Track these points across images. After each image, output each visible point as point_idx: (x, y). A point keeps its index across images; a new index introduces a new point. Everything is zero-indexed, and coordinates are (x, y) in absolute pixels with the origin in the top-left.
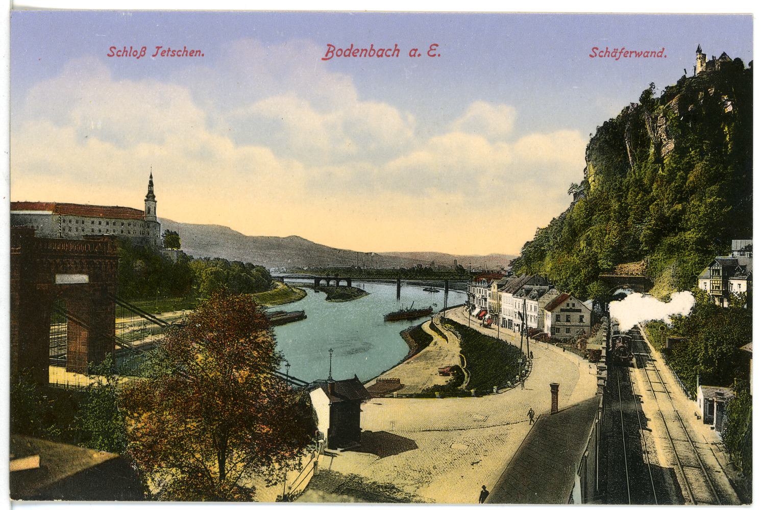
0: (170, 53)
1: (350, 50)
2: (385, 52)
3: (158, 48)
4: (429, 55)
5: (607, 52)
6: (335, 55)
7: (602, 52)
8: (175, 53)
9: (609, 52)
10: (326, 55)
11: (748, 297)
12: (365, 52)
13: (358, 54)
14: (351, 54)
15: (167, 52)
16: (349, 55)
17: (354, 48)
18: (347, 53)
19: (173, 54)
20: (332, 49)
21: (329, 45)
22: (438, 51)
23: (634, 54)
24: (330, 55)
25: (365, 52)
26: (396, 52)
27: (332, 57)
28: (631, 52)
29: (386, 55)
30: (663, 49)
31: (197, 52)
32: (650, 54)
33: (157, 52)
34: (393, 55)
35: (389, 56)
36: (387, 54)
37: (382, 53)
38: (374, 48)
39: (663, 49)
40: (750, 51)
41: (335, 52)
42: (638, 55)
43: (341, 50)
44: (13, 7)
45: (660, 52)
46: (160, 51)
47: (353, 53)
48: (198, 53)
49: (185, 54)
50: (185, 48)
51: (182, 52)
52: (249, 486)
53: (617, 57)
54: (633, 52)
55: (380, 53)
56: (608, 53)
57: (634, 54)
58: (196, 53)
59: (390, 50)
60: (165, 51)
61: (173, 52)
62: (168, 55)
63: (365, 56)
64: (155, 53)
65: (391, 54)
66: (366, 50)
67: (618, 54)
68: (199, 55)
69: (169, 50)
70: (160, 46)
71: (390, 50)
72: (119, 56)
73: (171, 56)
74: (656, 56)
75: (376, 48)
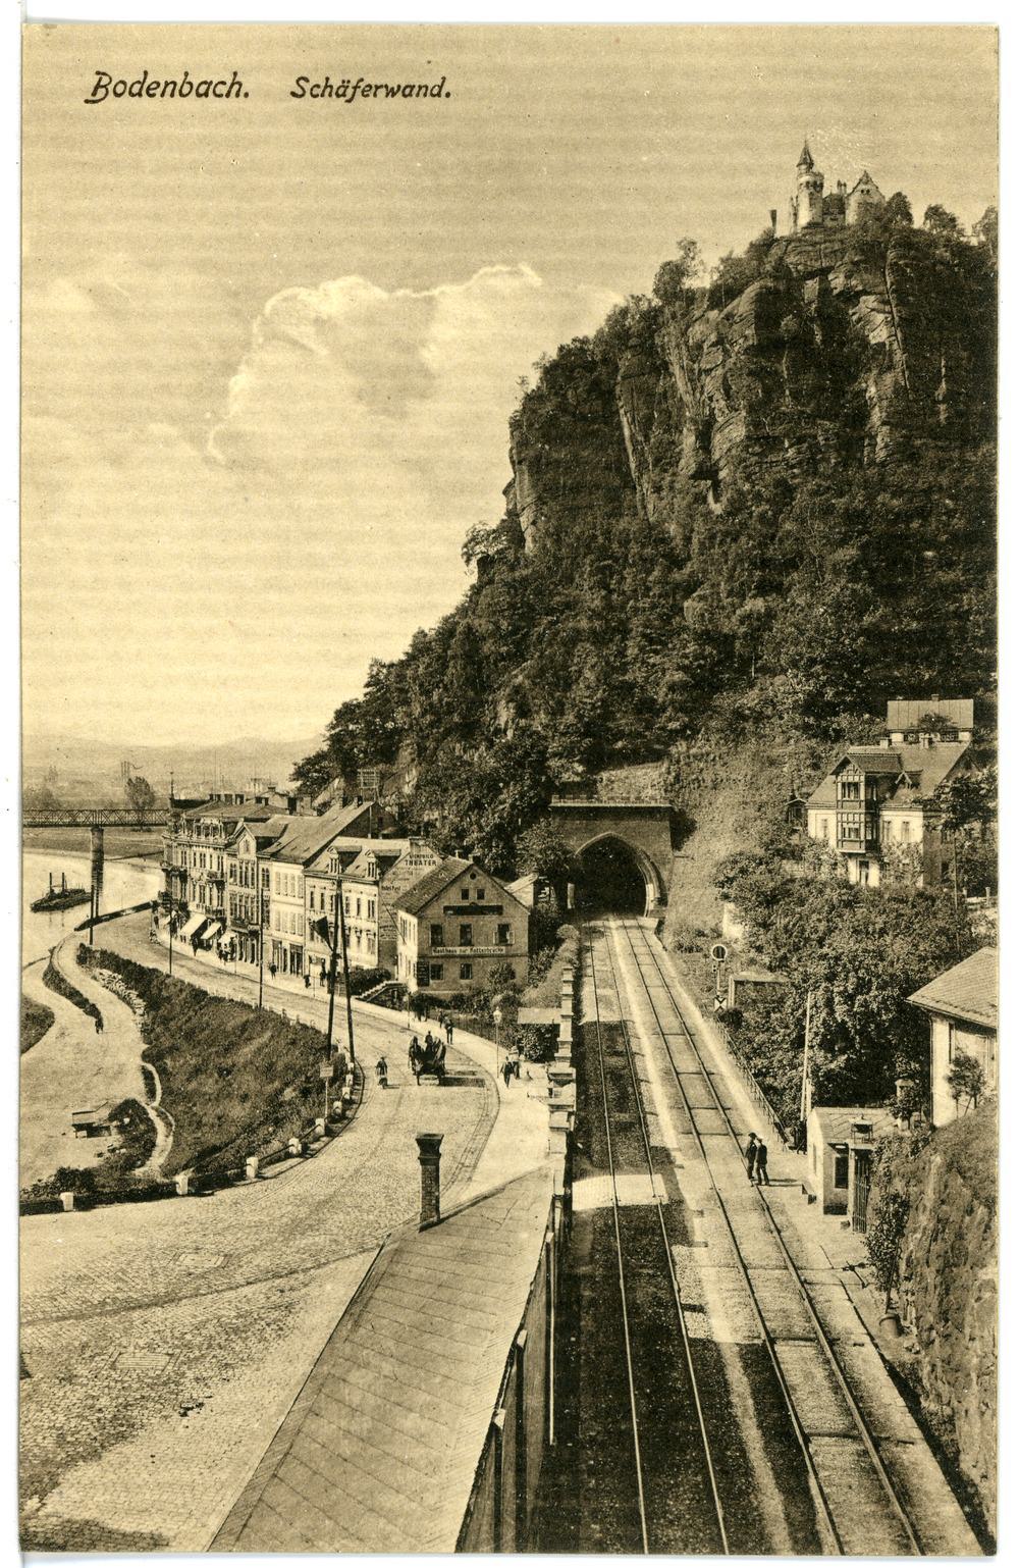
1: (441, 87)
2: (212, 87)
5: (326, 86)
8: (307, 87)
9: (331, 87)
10: (94, 94)
13: (159, 91)
16: (140, 94)
18: (135, 90)
19: (300, 92)
20: (105, 80)
21: (98, 73)
23: (382, 92)
24: (101, 92)
25: (171, 86)
26: (236, 87)
28: (377, 87)
29: (147, 93)
30: (444, 79)
32: (416, 90)
34: (228, 95)
35: (220, 96)
36: (218, 92)
37: (205, 90)
39: (444, 79)
41: (110, 87)
42: (391, 92)
47: (148, 88)
53: (349, 96)
54: (381, 86)
55: (203, 89)
56: (328, 90)
57: (382, 92)
59: (223, 83)
65: (225, 93)
67: (350, 92)
68: (237, 95)
71: (223, 83)
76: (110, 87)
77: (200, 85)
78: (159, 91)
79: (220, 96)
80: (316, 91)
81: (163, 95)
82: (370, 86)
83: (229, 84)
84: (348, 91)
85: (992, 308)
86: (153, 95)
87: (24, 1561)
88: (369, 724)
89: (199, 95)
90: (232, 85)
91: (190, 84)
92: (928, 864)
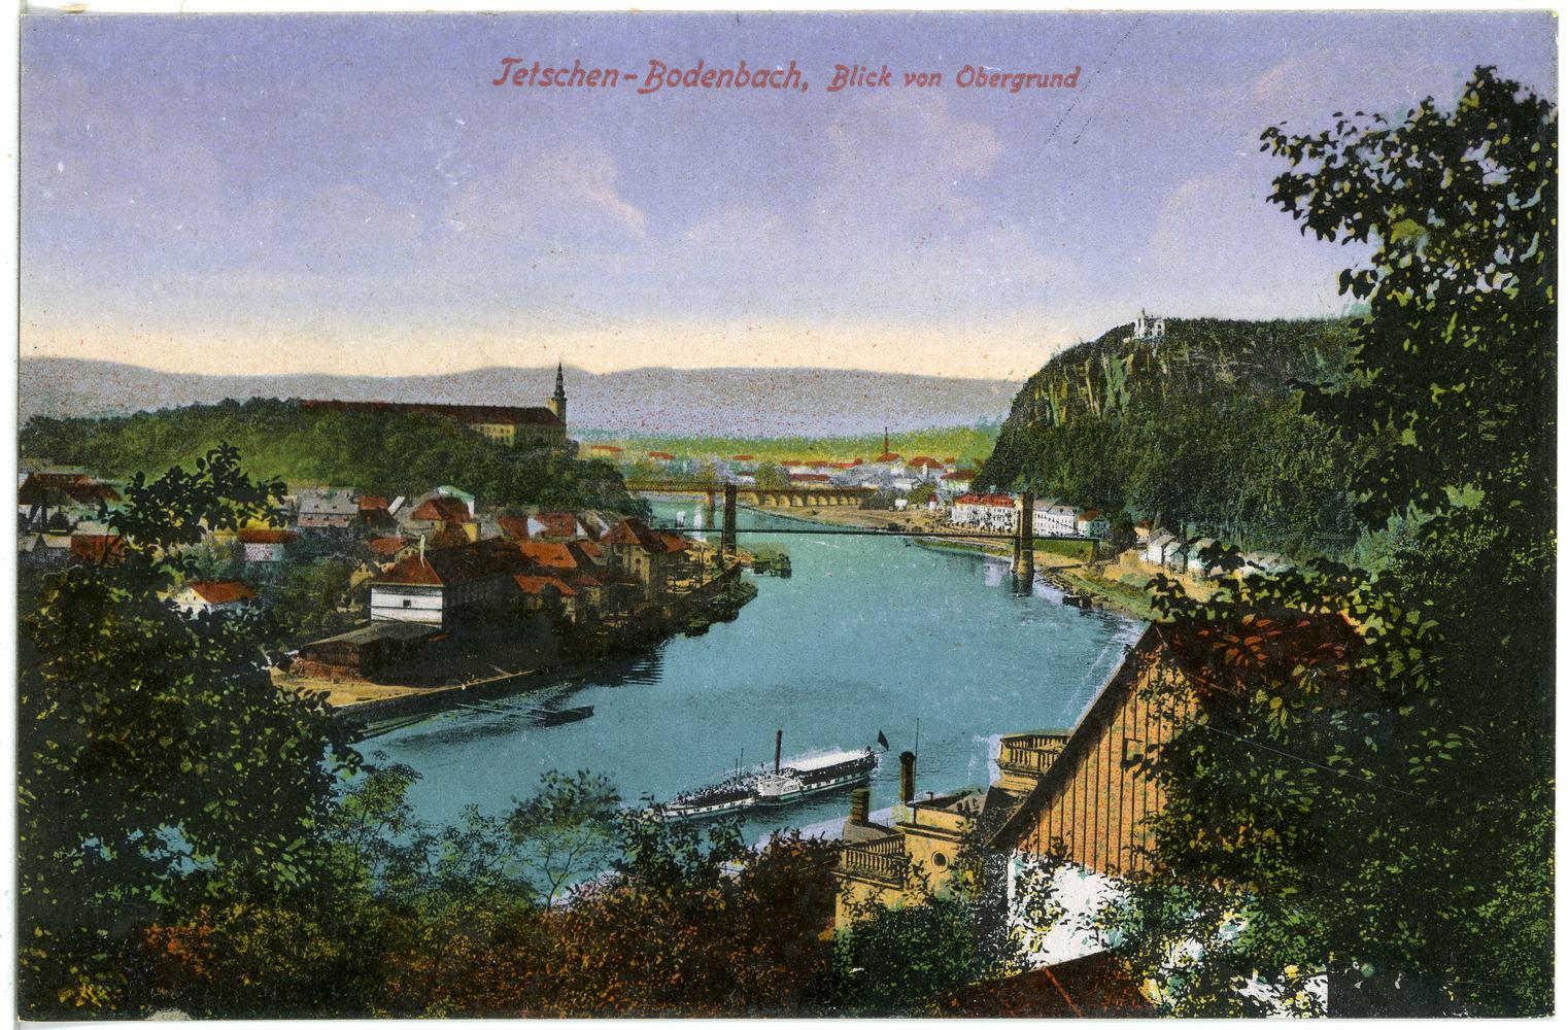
0: (540, 76)
3: (508, 61)
4: (964, 85)
5: (576, 71)
6: (665, 83)
7: (874, 75)
10: (648, 83)
11: (1143, 1009)
12: (612, 76)
13: (600, 81)
14: (699, 82)
15: (530, 75)
17: (704, 70)
18: (691, 78)
19: (546, 80)
21: (653, 63)
22: (889, 79)
24: (655, 82)
25: (726, 78)
26: (794, 77)
27: (658, 87)
28: (1006, 77)
29: (703, 82)
30: (1078, 69)
31: (723, 74)
33: (506, 75)
34: (570, 83)
36: (560, 80)
38: (582, 67)
39: (1078, 69)
40: (1555, 89)
41: (665, 77)
43: (677, 72)
44: (25, 10)
45: (693, 71)
46: (515, 68)
47: (704, 78)
48: (936, 79)
49: (609, 81)
50: (743, 64)
51: (570, 75)
52: (325, 755)
54: (1035, 76)
55: (760, 79)
56: (579, 76)
57: (1034, 82)
58: (606, 78)
59: (566, 71)
60: (525, 72)
61: (546, 72)
62: (531, 82)
63: (728, 84)
64: (499, 77)
65: (782, 82)
66: (730, 73)
68: (796, 85)
69: (536, 70)
70: (515, 56)
71: (566, 71)
72: (872, 84)
73: (542, 84)
74: (584, 82)
75: (752, 69)
76: (665, 77)
77: (687, 74)
78: (528, 79)
79: (562, 84)
80: (872, 79)
81: (604, 84)
82: (713, 73)
83: (571, 71)
84: (701, 77)
85: (693, 1001)
86: (593, 84)
87: (17, 1025)
88: (182, 735)
89: (755, 85)
90: (790, 75)
91: (747, 73)
92: (1203, 959)
